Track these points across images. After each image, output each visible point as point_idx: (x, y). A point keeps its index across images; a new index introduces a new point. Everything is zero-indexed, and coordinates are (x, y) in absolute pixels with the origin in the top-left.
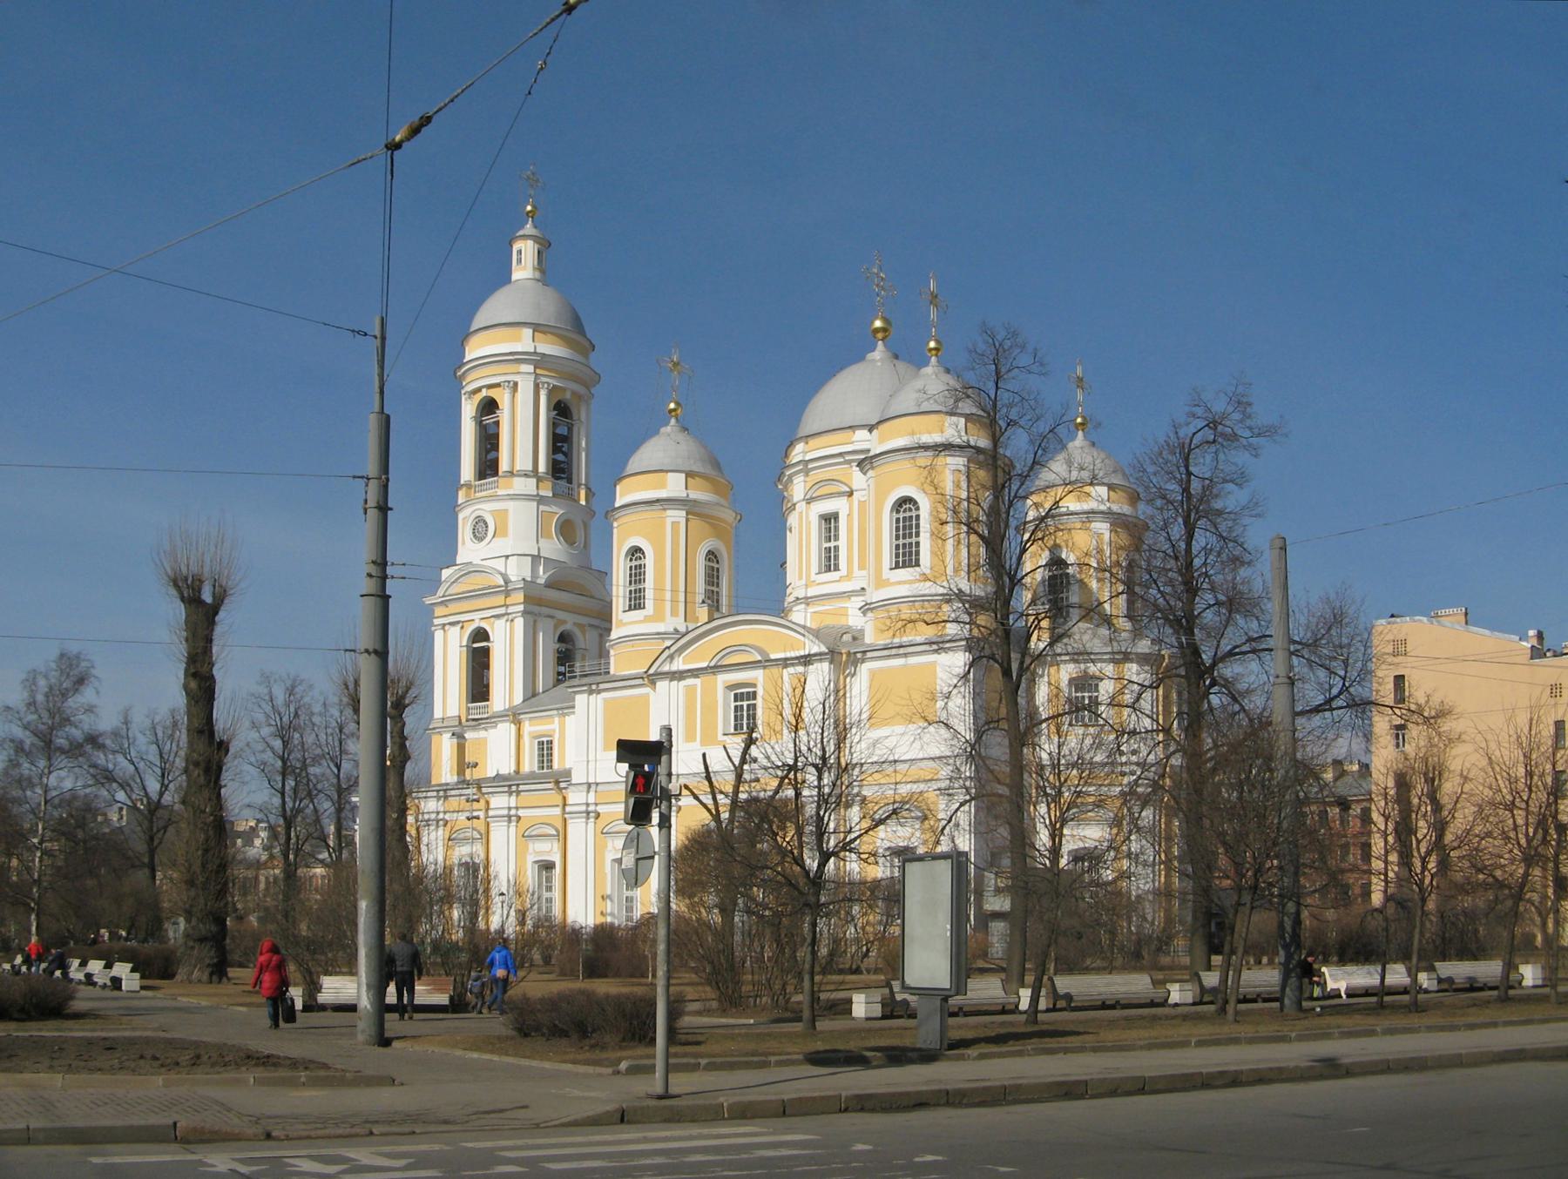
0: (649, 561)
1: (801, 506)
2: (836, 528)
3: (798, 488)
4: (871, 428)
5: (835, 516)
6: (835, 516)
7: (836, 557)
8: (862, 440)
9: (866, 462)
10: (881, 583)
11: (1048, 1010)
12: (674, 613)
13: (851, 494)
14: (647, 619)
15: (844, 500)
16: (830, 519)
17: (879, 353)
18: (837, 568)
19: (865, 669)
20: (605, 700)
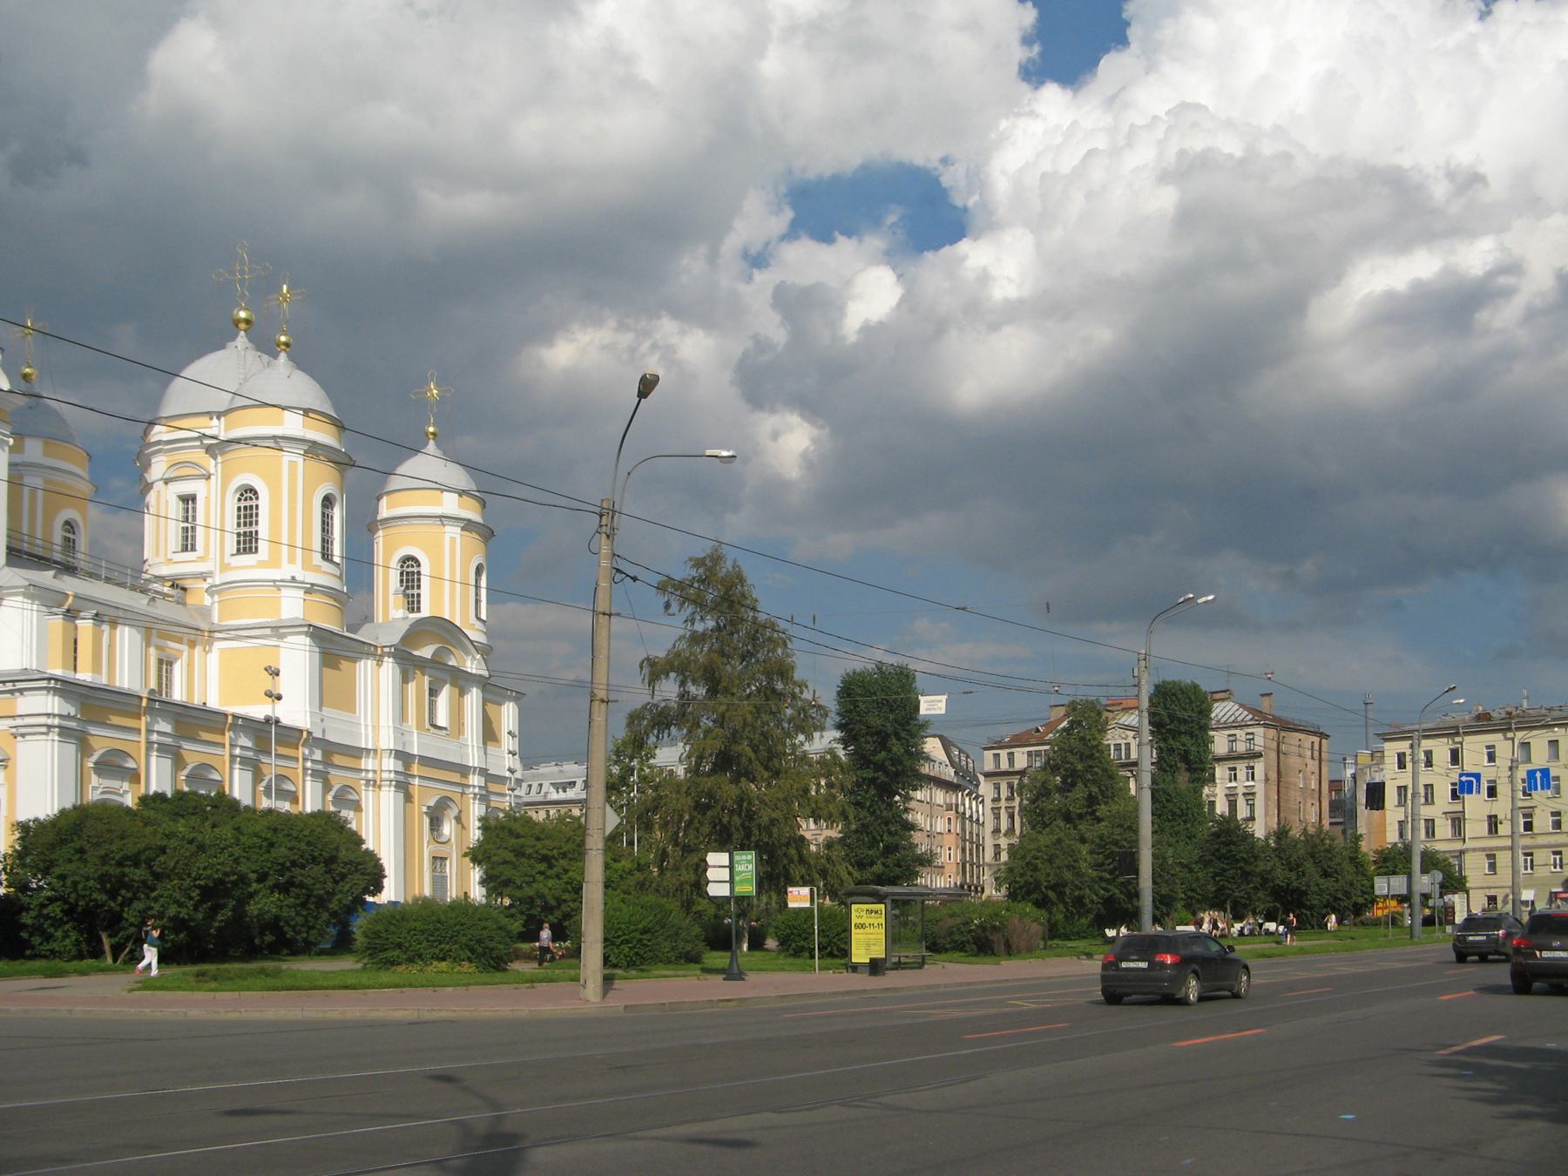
0: (264, 503)
1: (159, 485)
2: (194, 509)
3: (159, 468)
4: (219, 415)
5: (193, 498)
6: (193, 498)
7: (193, 538)
8: (217, 428)
9: (217, 448)
10: (225, 567)
11: (875, 967)
12: (292, 560)
13: (208, 478)
14: (261, 565)
15: (202, 483)
16: (188, 499)
17: (242, 339)
18: (193, 549)
19: (218, 645)
20: (222, 650)
